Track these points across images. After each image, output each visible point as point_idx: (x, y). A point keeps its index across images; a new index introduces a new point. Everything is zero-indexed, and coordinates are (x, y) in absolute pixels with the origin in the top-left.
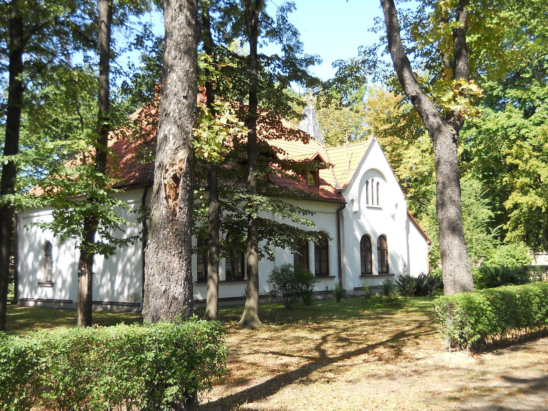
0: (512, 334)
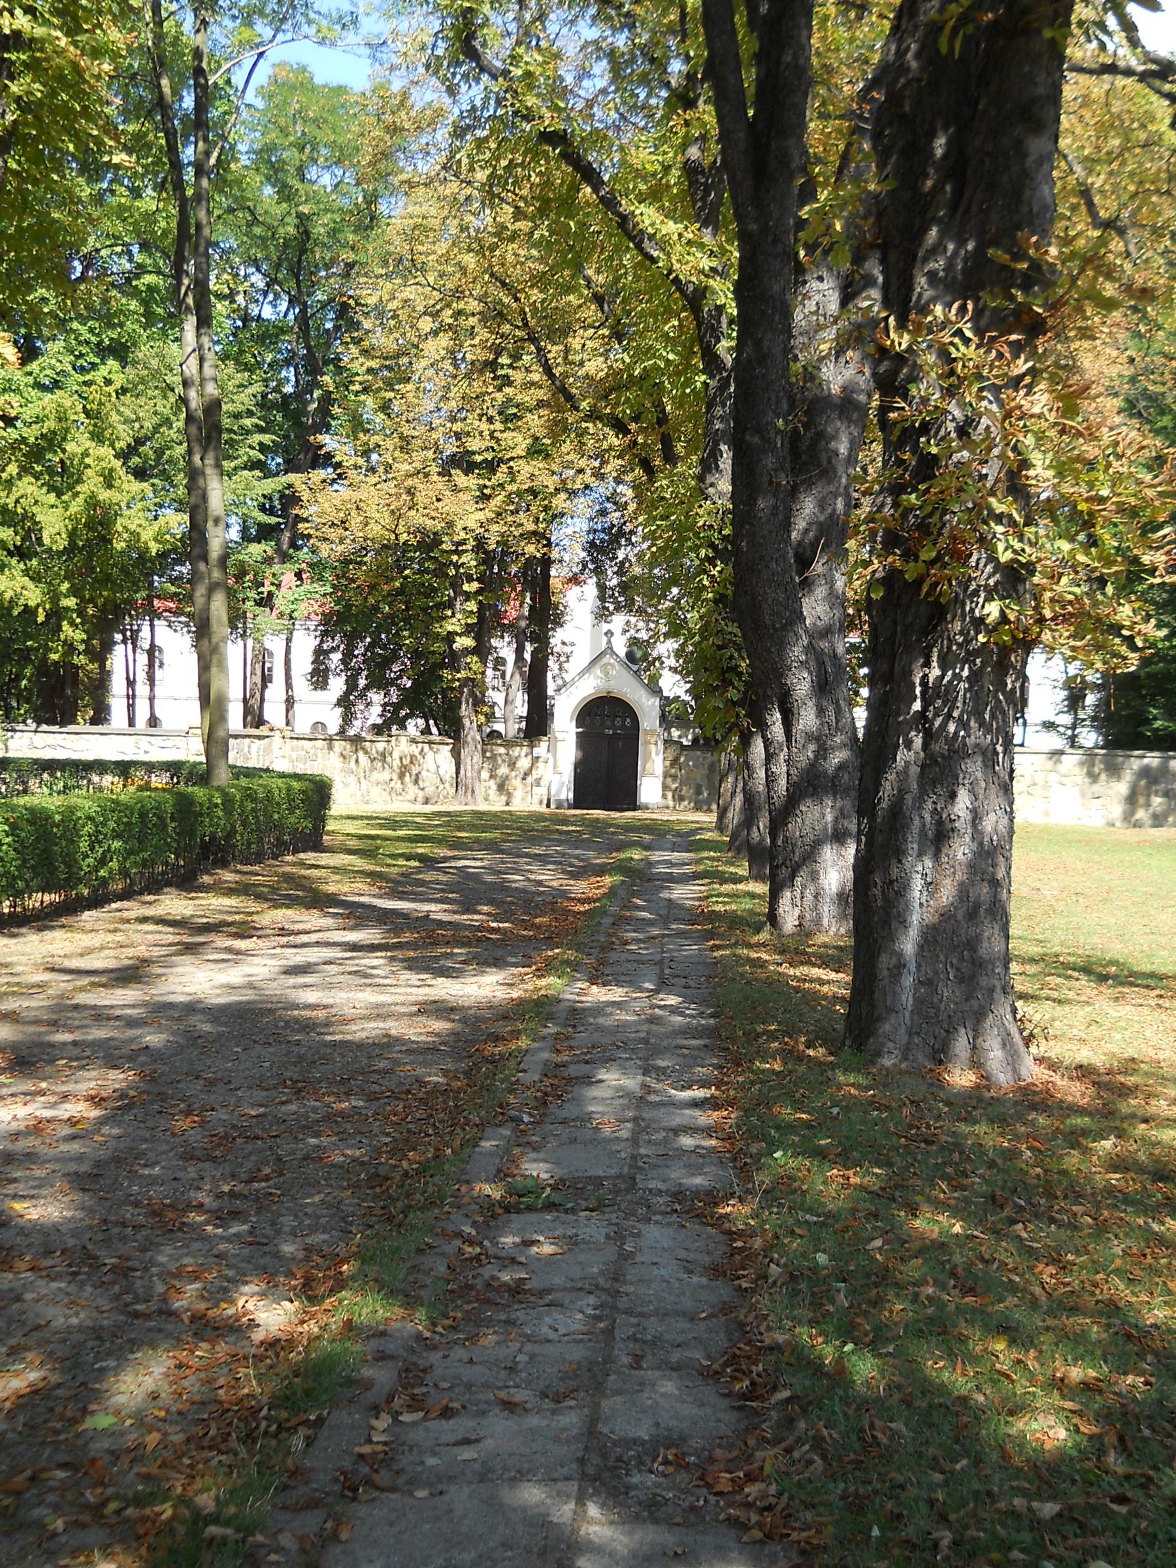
0: (37, 900)
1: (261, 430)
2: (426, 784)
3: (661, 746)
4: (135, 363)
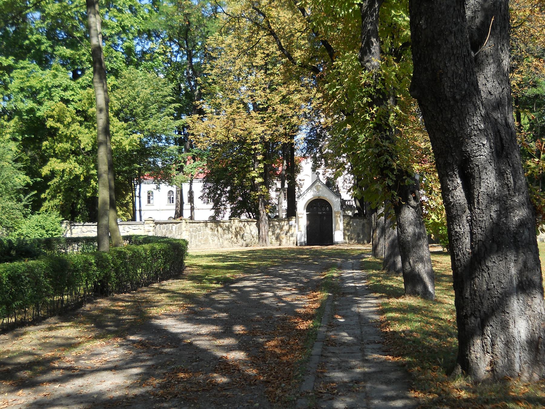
1: (174, 102)
2: (246, 239)
3: (342, 217)
4: (121, 77)
